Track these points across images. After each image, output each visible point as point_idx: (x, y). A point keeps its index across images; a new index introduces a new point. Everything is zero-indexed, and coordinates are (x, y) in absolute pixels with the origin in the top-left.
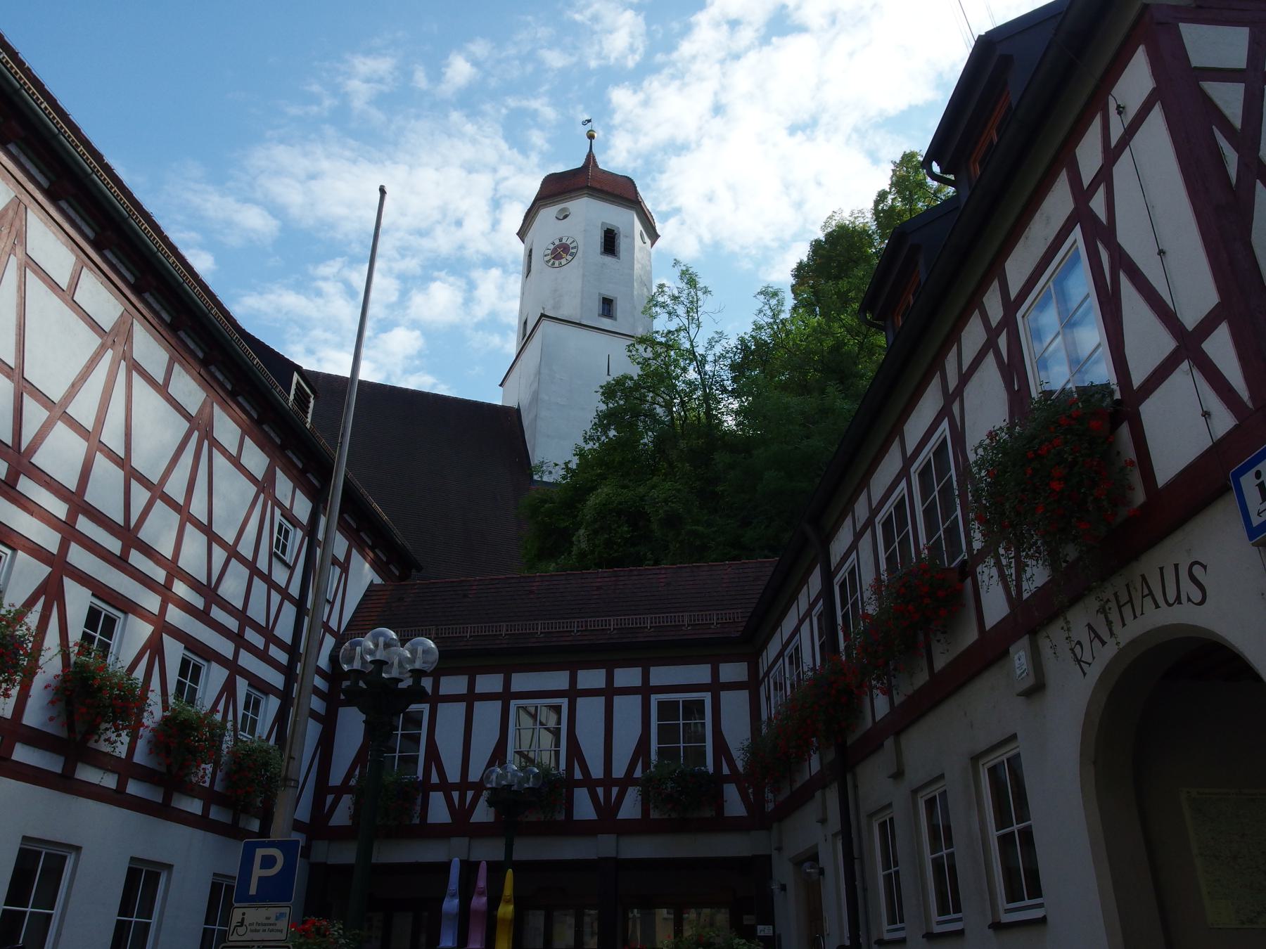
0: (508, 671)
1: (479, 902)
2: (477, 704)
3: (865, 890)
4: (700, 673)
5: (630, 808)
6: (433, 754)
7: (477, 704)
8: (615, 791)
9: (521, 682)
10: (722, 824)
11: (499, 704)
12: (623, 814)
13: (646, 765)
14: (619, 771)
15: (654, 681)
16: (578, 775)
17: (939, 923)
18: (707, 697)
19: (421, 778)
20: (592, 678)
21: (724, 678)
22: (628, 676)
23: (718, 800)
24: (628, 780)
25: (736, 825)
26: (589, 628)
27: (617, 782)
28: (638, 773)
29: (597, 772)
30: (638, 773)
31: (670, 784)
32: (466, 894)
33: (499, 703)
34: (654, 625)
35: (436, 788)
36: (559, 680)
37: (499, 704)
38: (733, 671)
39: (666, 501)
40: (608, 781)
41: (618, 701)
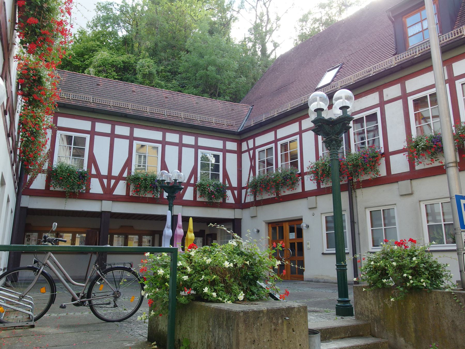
0: (94, 121)
1: (180, 231)
2: (109, 138)
3: (359, 234)
4: (86, 125)
5: (120, 190)
6: (92, 159)
7: (109, 138)
8: (113, 182)
9: (139, 132)
10: (224, 205)
11: (116, 140)
12: (116, 193)
13: (129, 173)
14: (116, 172)
15: (200, 144)
16: (94, 172)
17: (372, 249)
18: (88, 137)
19: (86, 170)
20: (172, 137)
21: (228, 148)
22: (188, 139)
23: (224, 197)
24: (119, 178)
25: (230, 206)
26: (171, 115)
27: (114, 178)
28: (125, 175)
29: (235, 184)
30: (125, 175)
31: (211, 187)
32: (174, 227)
33: (96, 137)
34: (132, 108)
35: (94, 176)
36: (158, 135)
37: (116, 140)
38: (232, 146)
39: (148, 66)
40: (109, 177)
41: (167, 147)
